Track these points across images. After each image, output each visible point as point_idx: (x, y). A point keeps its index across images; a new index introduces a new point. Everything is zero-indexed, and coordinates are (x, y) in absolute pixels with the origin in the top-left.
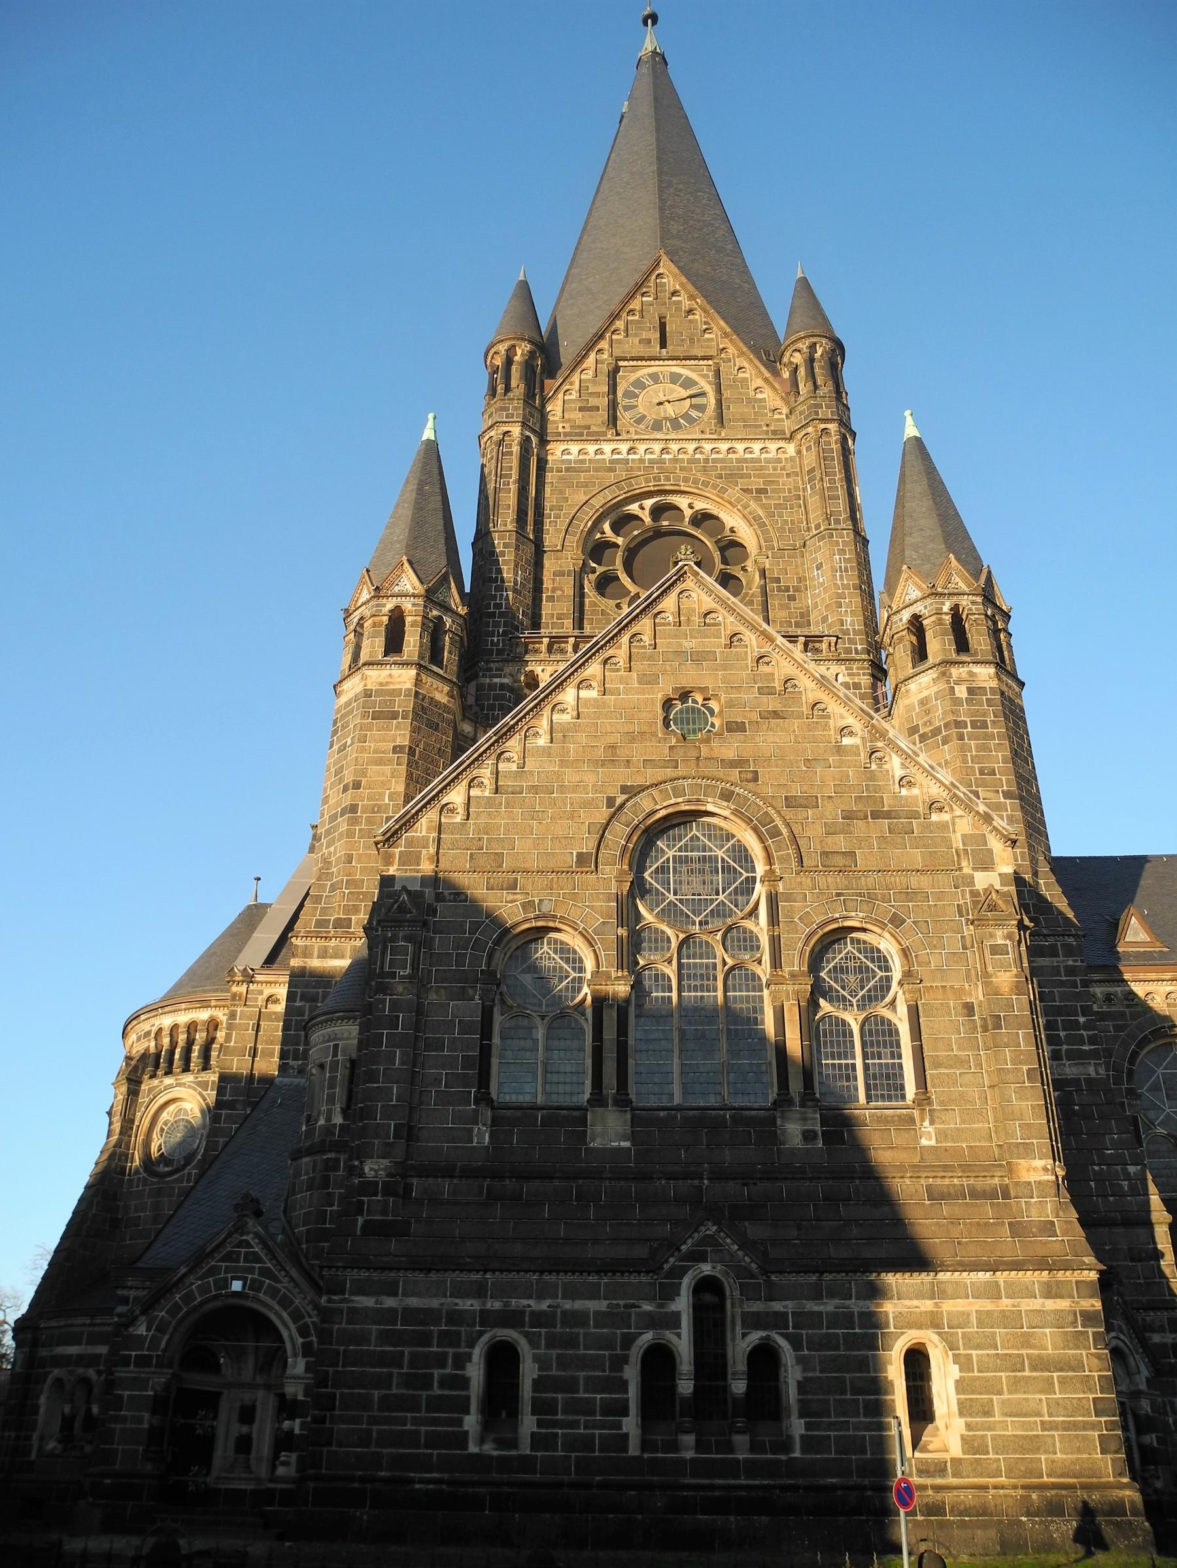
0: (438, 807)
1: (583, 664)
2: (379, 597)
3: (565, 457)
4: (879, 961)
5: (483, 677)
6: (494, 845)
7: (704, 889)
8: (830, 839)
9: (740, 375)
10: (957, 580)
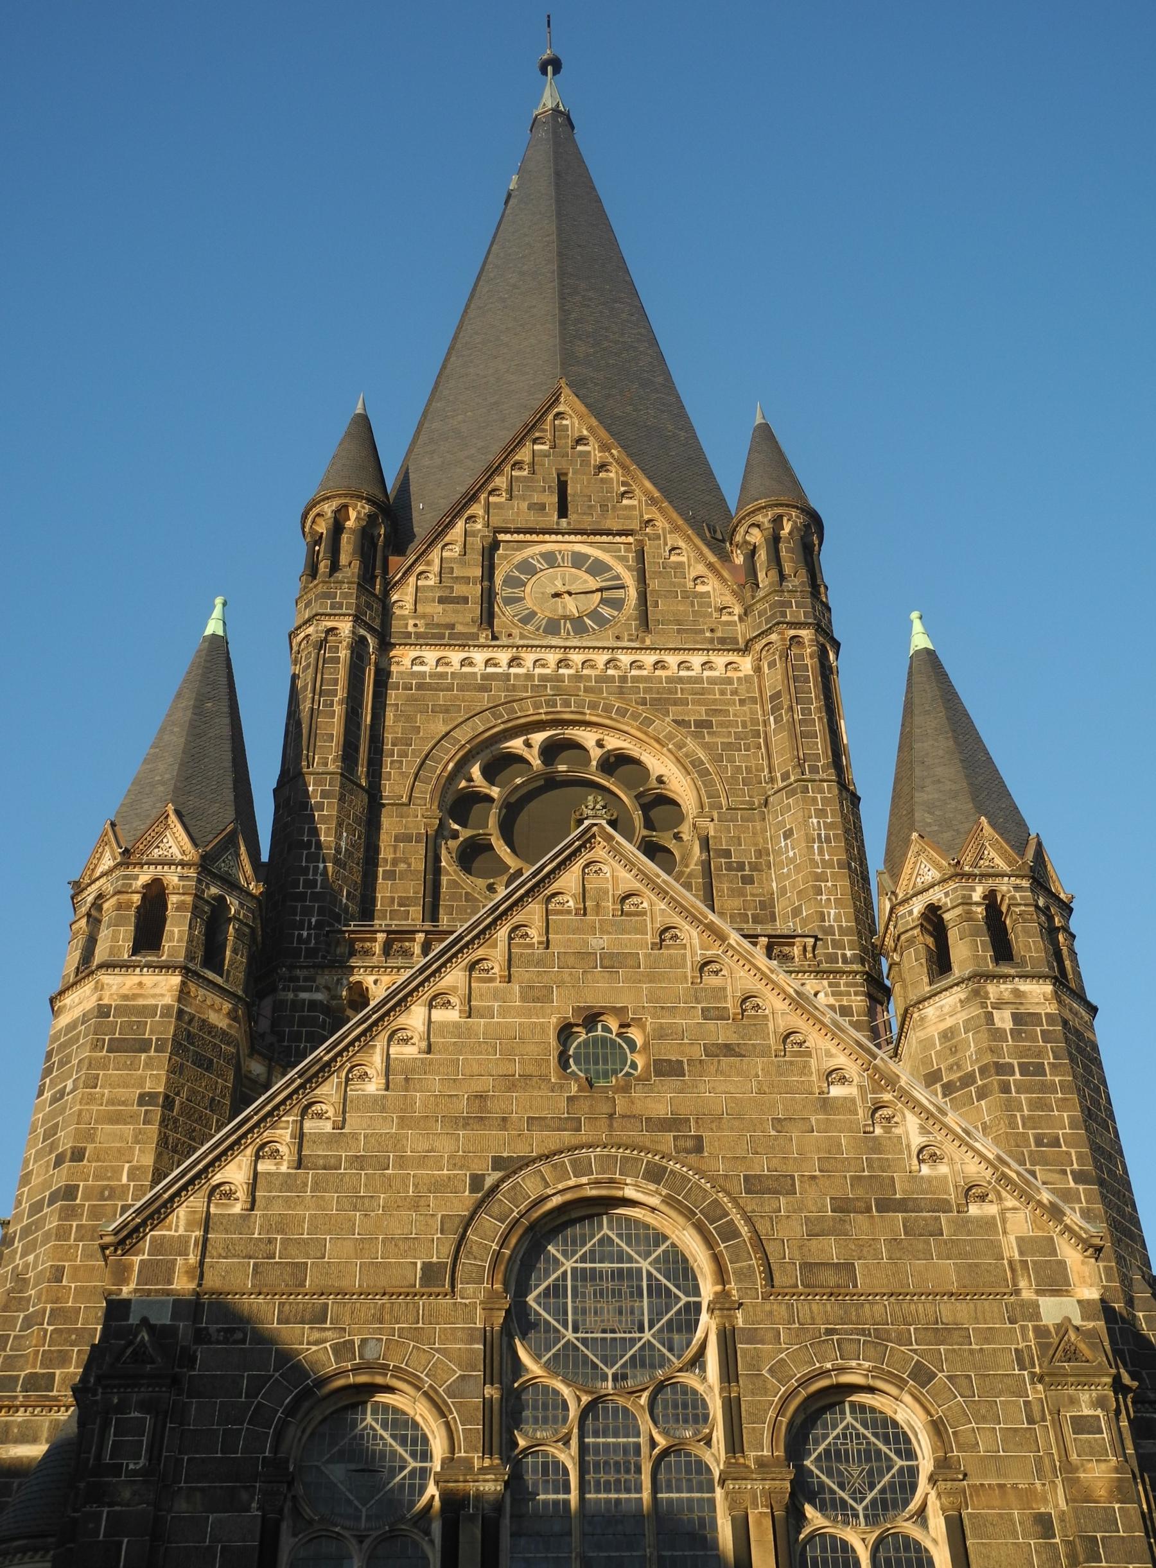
0: (206, 1189)
1: (438, 970)
2: (128, 865)
3: (416, 668)
4: (897, 1442)
5: (283, 990)
6: (293, 1250)
7: (620, 1322)
8: (814, 1244)
9: (673, 558)
10: (993, 854)
